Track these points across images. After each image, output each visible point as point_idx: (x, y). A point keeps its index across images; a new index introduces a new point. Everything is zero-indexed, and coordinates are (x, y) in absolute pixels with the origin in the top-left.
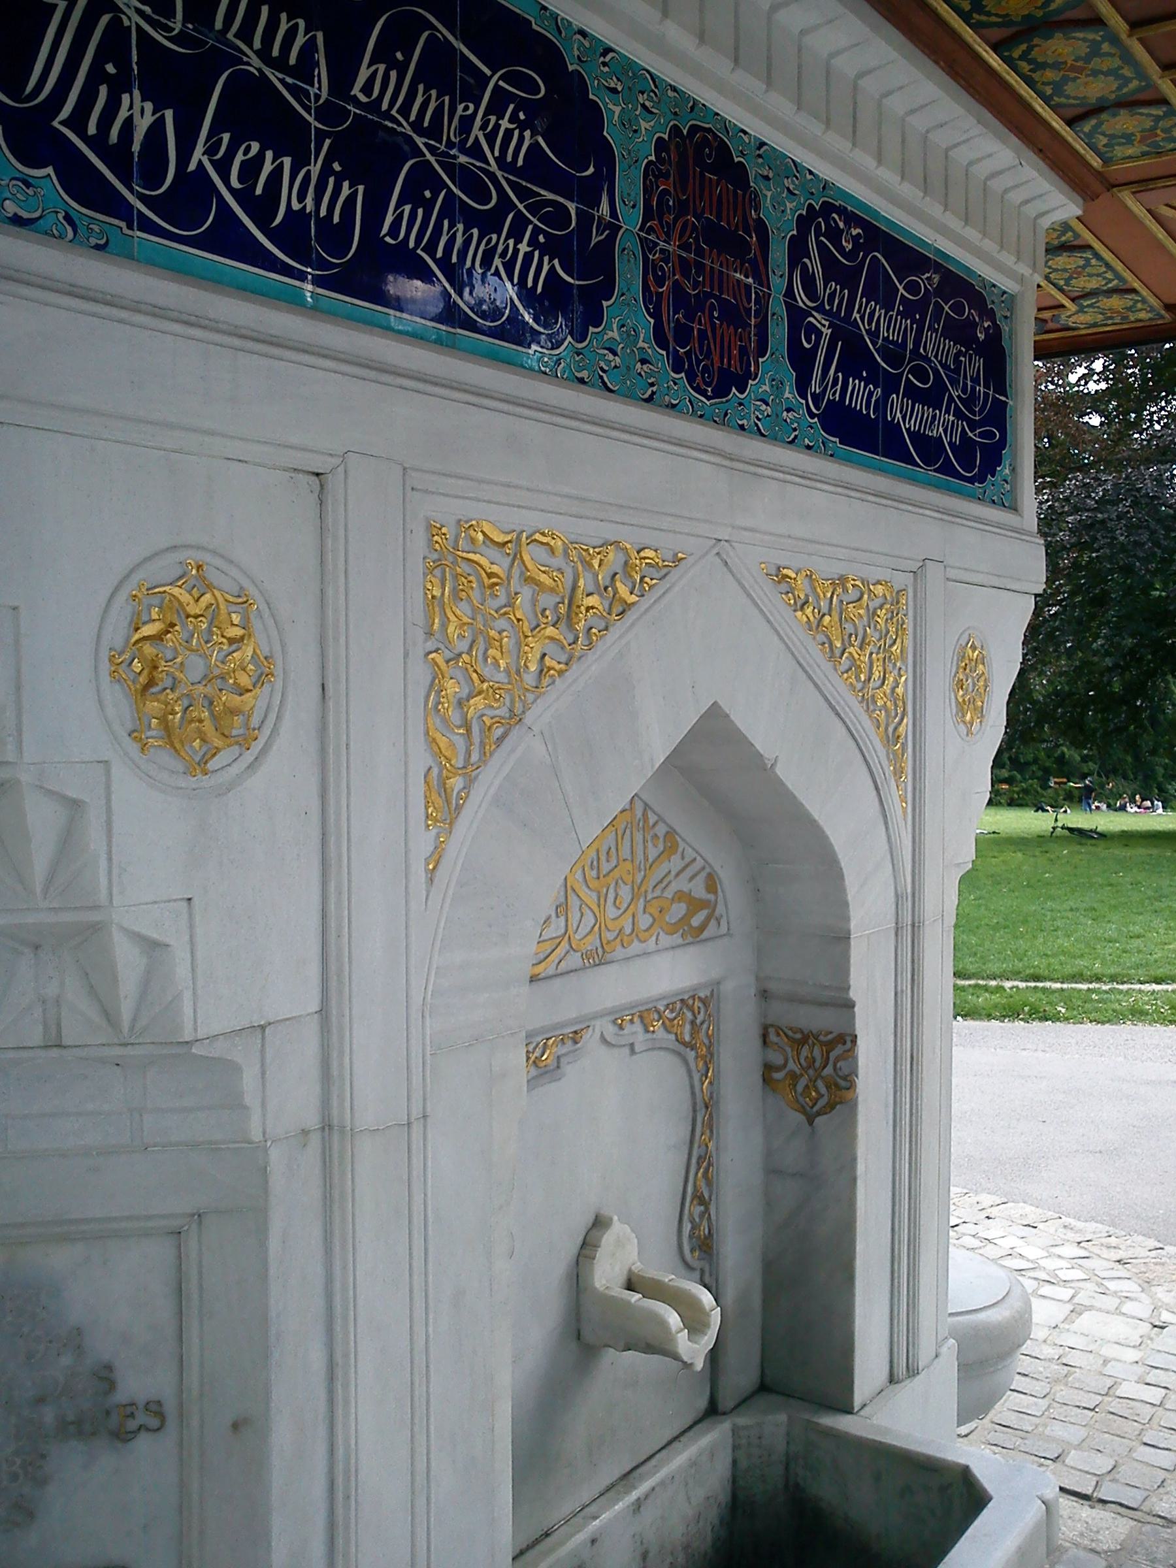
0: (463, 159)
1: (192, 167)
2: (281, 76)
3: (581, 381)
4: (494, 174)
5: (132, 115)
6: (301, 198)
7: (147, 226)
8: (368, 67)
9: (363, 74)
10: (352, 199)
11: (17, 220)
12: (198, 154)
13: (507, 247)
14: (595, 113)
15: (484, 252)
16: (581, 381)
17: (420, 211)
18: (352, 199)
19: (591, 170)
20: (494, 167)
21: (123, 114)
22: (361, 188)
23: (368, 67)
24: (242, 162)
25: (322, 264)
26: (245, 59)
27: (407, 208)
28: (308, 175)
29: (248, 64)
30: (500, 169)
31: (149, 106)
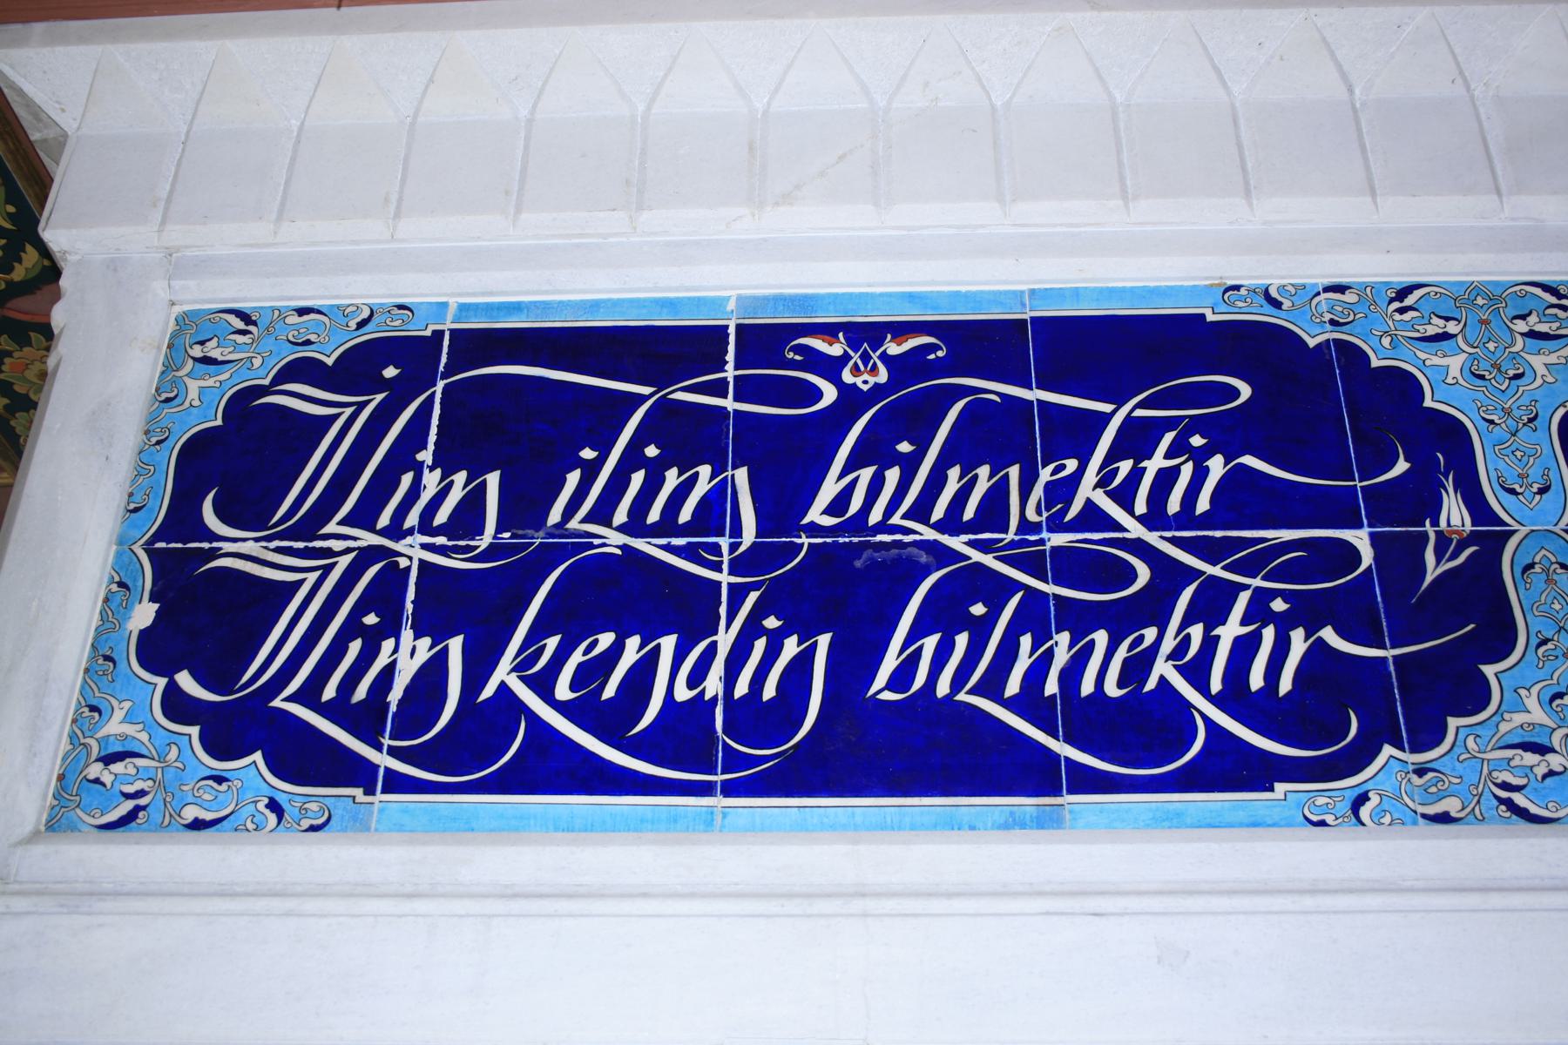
0: (1059, 539)
1: (488, 691)
2: (663, 541)
3: (1444, 818)
4: (1139, 540)
5: (395, 661)
6: (696, 678)
7: (395, 783)
8: (841, 477)
9: (829, 489)
10: (804, 661)
11: (197, 825)
12: (503, 673)
13: (1187, 640)
14: (1403, 385)
15: (1126, 661)
16: (1444, 818)
17: (1256, 681)
18: (804, 661)
19: (1402, 466)
20: (1135, 530)
21: (382, 661)
22: (493, 480)
23: (841, 477)
24: (580, 666)
25: (734, 761)
26: (596, 542)
27: (930, 643)
28: (713, 648)
29: (604, 545)
30: (978, 565)
31: (426, 642)
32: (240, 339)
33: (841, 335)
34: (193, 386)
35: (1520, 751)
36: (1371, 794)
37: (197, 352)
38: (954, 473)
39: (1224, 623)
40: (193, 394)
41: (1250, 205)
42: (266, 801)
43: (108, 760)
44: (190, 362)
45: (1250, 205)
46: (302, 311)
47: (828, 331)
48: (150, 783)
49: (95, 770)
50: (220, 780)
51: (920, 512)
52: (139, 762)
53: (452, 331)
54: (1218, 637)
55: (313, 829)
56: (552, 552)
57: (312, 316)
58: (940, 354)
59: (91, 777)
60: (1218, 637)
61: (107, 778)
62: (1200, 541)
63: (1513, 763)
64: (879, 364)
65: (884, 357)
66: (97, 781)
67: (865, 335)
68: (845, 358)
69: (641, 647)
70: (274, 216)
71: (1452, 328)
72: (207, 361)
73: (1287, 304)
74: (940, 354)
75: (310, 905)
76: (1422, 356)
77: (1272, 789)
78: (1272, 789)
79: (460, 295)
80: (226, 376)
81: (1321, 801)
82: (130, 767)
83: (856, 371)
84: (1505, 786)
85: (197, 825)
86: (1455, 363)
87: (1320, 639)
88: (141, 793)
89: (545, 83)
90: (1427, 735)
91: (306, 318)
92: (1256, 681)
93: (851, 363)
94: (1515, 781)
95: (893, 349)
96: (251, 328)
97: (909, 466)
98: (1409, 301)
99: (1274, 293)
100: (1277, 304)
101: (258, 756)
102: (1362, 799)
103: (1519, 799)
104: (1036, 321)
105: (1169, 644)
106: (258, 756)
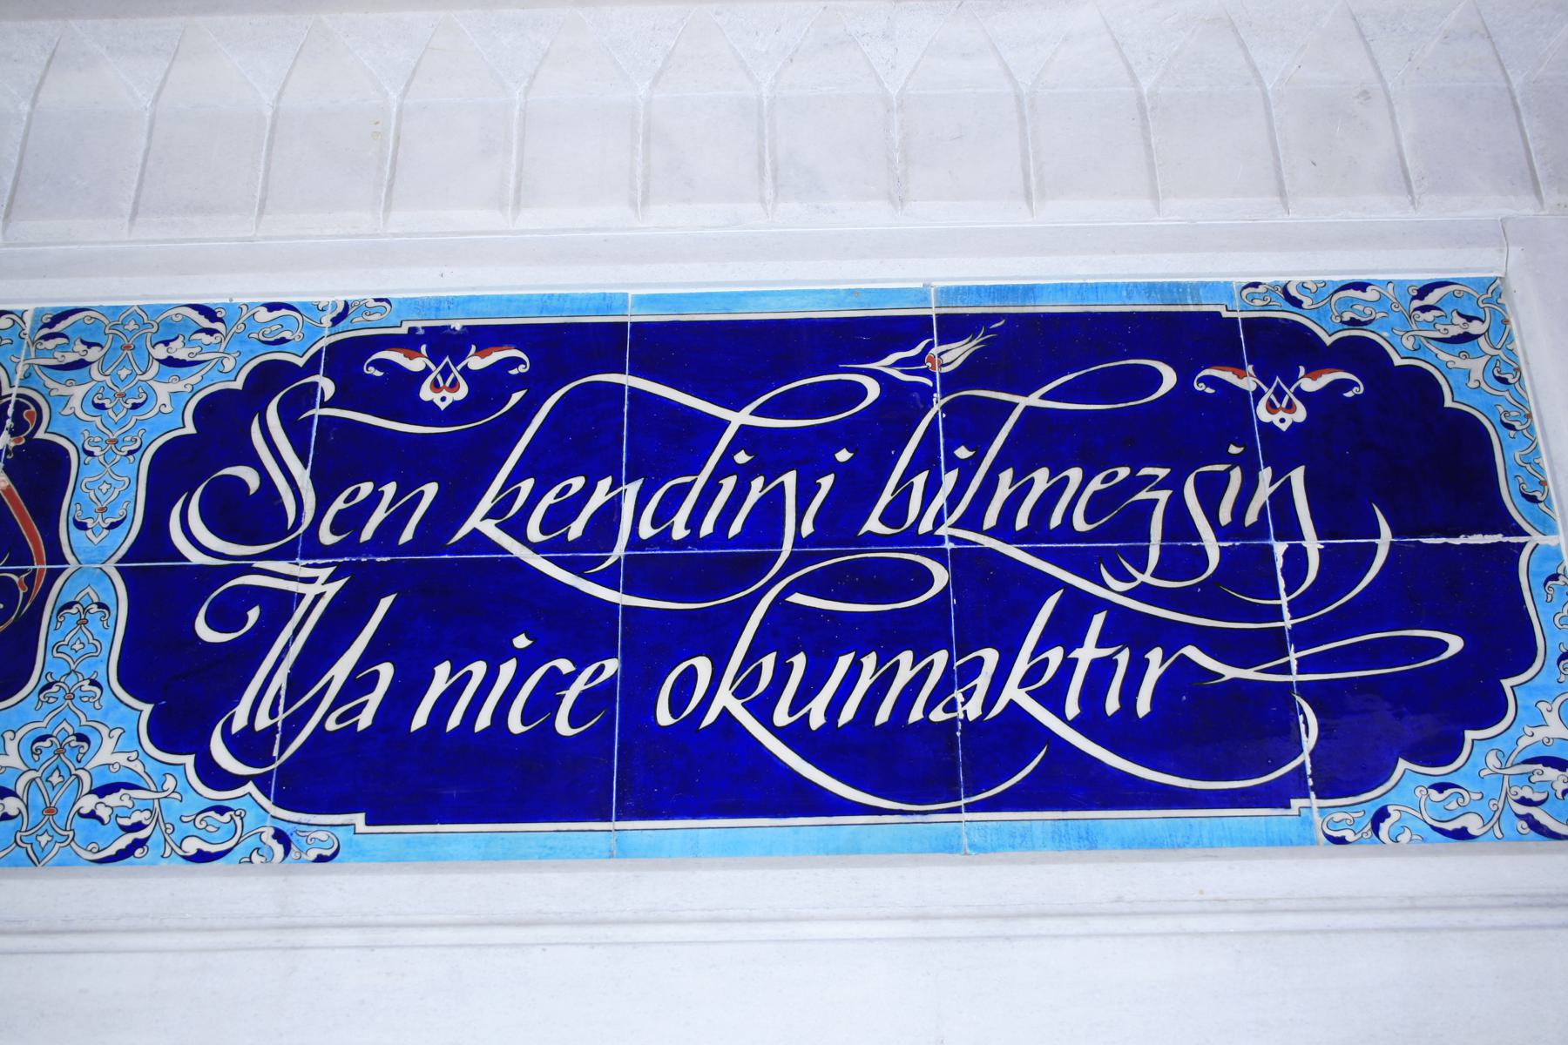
11: (201, 857)
16: (1462, 834)
17: (1112, 704)
32: (205, 338)
33: (423, 349)
34: (163, 391)
35: (1540, 766)
36: (1390, 809)
37: (161, 352)
38: (1006, 476)
39: (1081, 645)
40: (163, 397)
41: (1030, 205)
42: (272, 831)
43: (103, 791)
44: (156, 364)
45: (1030, 205)
46: (272, 307)
47: (409, 342)
48: (147, 814)
49: (88, 803)
50: (221, 810)
51: (972, 520)
52: (135, 793)
53: (939, 317)
54: (1076, 660)
55: (321, 859)
56: (535, 565)
57: (284, 312)
58: (522, 369)
59: (85, 811)
60: (1076, 660)
61: (103, 812)
62: (1215, 545)
63: (1533, 779)
64: (460, 378)
65: (466, 372)
66: (92, 815)
67: (444, 344)
68: (427, 371)
69: (451, 675)
70: (127, 208)
71: (1475, 328)
72: (171, 362)
73: (1307, 303)
74: (522, 369)
75: (315, 938)
76: (1443, 357)
77: (1288, 807)
78: (1288, 807)
79: (36, 301)
80: (195, 379)
81: (1338, 816)
82: (126, 798)
83: (436, 386)
84: (1524, 801)
85: (201, 857)
86: (1476, 366)
87: (1183, 658)
88: (139, 826)
89: (418, 63)
90: (1441, 750)
91: (276, 314)
92: (1112, 704)
93: (431, 378)
94: (1536, 797)
95: (476, 362)
96: (218, 326)
97: (967, 471)
98: (1431, 299)
99: (1293, 292)
100: (1297, 303)
101: (1507, 684)
102: (1381, 815)
103: (1539, 814)
104: (637, 326)
105: (1021, 666)
106: (1507, 684)
